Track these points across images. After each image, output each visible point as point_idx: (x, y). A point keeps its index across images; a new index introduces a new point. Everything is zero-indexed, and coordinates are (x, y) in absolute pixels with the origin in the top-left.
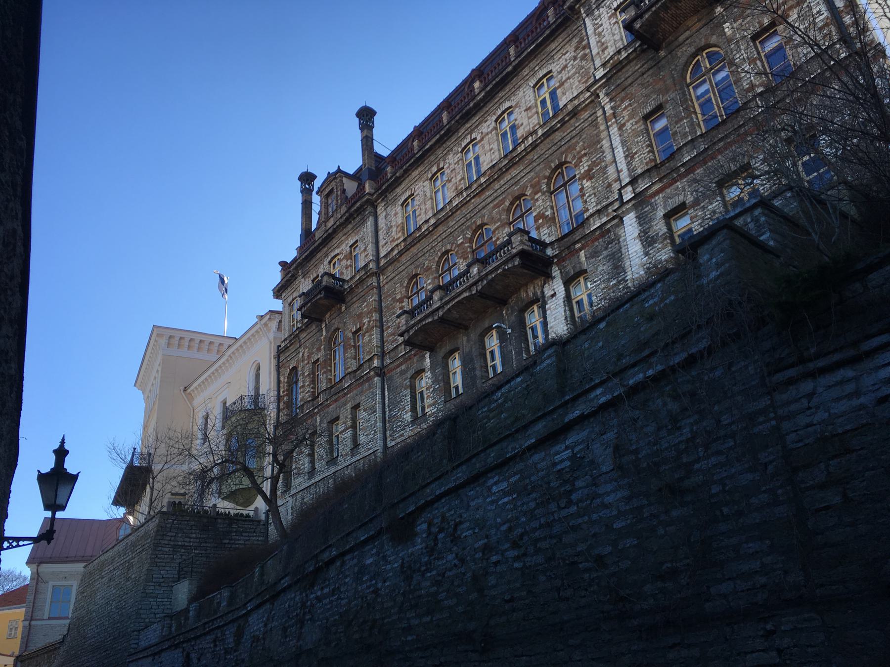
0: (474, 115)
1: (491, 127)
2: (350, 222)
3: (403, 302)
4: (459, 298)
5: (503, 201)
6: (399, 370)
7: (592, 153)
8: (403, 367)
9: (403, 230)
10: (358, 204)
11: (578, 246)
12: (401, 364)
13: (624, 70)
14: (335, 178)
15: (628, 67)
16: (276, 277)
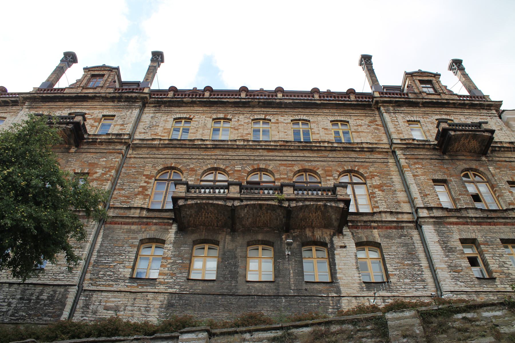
0: (273, 108)
1: (286, 121)
2: (113, 102)
3: (150, 179)
4: (215, 202)
5: (292, 166)
6: (126, 227)
7: (383, 178)
8: (134, 227)
9: (170, 133)
10: (134, 95)
11: (373, 224)
12: (133, 224)
13: (418, 150)
14: (111, 71)
15: (421, 150)
16: (85, 67)
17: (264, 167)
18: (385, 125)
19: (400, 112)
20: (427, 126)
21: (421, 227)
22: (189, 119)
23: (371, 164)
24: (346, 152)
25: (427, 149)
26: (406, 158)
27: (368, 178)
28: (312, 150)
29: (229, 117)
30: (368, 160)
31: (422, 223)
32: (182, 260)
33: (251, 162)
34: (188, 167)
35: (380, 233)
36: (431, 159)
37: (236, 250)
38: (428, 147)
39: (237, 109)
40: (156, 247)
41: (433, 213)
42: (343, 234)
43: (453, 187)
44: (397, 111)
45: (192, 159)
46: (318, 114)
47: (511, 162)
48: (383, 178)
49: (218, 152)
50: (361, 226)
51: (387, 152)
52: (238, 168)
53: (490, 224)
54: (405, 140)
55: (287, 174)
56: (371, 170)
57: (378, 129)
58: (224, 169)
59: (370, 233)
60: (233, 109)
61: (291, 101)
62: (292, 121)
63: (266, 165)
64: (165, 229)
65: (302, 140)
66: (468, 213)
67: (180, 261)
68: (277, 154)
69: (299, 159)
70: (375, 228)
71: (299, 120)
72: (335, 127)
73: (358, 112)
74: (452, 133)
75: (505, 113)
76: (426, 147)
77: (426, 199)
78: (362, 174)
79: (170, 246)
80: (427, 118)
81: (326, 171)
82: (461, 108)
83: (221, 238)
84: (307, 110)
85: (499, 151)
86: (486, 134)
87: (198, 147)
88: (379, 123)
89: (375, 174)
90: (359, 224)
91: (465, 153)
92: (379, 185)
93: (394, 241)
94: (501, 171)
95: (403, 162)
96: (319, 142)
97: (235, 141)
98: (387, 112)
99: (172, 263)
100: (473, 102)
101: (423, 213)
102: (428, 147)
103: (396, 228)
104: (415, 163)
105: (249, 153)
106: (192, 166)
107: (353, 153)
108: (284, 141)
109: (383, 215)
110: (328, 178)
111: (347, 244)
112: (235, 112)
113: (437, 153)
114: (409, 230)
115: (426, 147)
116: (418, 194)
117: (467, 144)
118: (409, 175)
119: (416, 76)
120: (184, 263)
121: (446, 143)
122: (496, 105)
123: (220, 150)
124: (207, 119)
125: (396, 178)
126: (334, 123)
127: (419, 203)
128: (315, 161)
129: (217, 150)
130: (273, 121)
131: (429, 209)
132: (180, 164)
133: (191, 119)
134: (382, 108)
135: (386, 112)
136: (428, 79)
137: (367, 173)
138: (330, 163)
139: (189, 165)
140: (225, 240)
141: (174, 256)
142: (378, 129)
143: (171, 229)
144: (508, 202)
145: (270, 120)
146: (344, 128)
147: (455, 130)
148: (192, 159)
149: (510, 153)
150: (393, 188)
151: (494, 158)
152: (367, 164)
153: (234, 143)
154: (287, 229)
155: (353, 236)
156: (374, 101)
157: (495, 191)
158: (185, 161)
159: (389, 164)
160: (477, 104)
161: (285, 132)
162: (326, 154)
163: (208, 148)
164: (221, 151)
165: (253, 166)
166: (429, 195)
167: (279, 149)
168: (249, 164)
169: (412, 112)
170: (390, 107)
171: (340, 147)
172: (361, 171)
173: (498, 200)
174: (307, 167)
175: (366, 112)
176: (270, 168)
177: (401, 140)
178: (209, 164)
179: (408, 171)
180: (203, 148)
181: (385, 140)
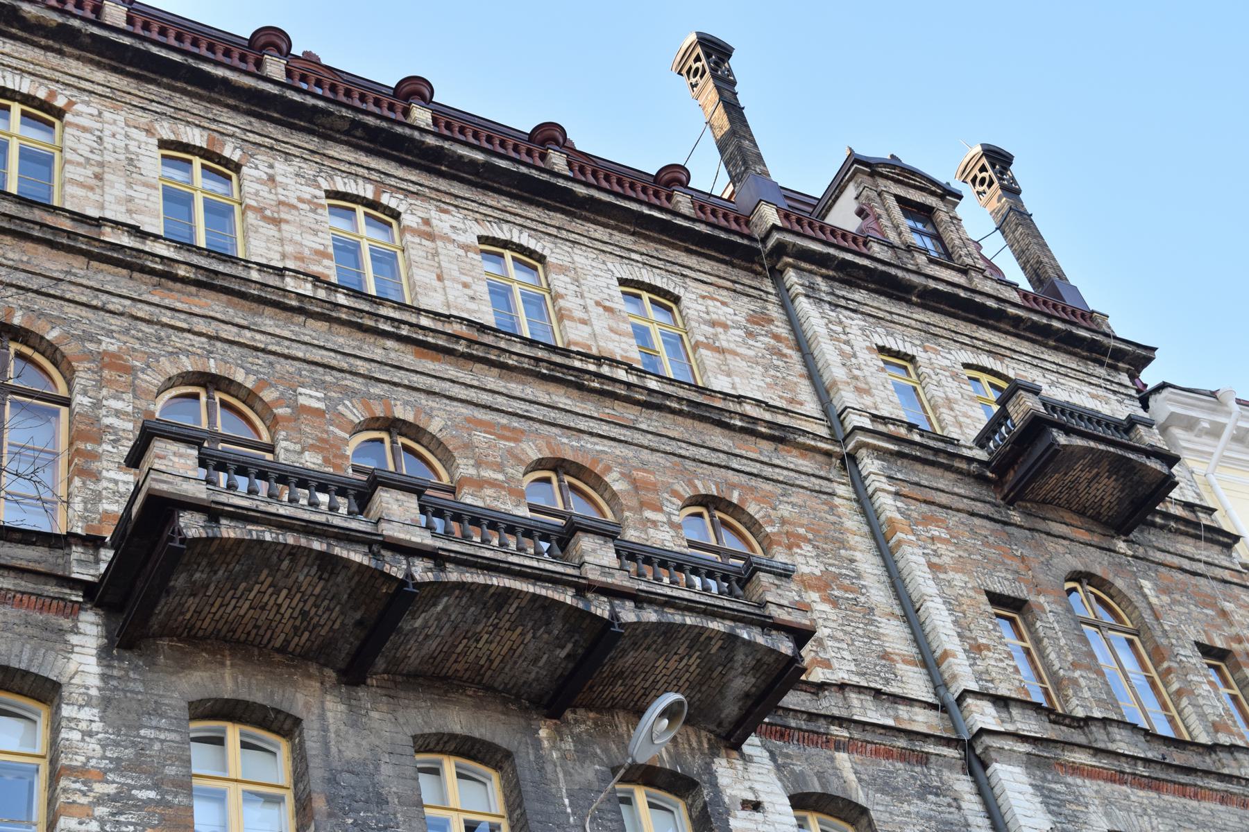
1: (462, 238)
5: (516, 436)
11: (835, 730)
13: (929, 469)
15: (939, 472)
17: (410, 417)
18: (803, 345)
19: (852, 305)
20: (939, 384)
21: (985, 766)
22: (45, 106)
23: (778, 489)
24: (696, 423)
25: (958, 471)
26: (897, 494)
27: (779, 544)
28: (580, 387)
29: (230, 151)
30: (768, 471)
31: (993, 755)
32: (156, 786)
33: (357, 384)
34: (91, 346)
35: (859, 768)
36: (972, 514)
37: (377, 767)
38: (964, 466)
39: (257, 125)
40: (245, 745)
41: (1012, 721)
42: (743, 756)
43: (1050, 633)
44: (843, 302)
45: (102, 309)
46: (572, 237)
47: (1194, 574)
48: (825, 552)
49: (214, 305)
50: (800, 730)
51: (828, 454)
52: (310, 398)
53: (1182, 790)
54: (884, 420)
55: (500, 467)
56: (786, 514)
57: (782, 355)
58: (250, 392)
59: (828, 764)
60: (240, 120)
61: (480, 157)
62: (482, 239)
63: (419, 410)
64: (45, 627)
65: (201, 242)
66: (1113, 741)
67: (152, 794)
68: (452, 372)
69: (535, 412)
70: (839, 746)
71: (506, 244)
72: (340, 224)
73: (707, 265)
74: (1062, 439)
75: (1166, 393)
76: (957, 464)
77: (981, 665)
78: (756, 522)
79: (86, 714)
80: (937, 352)
81: (636, 485)
82: (1033, 341)
83: (307, 705)
84: (533, 212)
85: (1162, 527)
86: (1154, 464)
87: (576, 383)
88: (783, 330)
89: (802, 531)
90: (793, 723)
91: (1068, 516)
92: (818, 578)
93: (906, 807)
94: (1174, 602)
95: (887, 505)
96: (599, 360)
97: (280, 272)
98: (811, 293)
99: (112, 798)
100: (1075, 330)
101: (983, 716)
102: (964, 466)
103: (904, 756)
104: (926, 520)
105: (343, 339)
106: (109, 345)
107: (718, 430)
108: (471, 323)
109: (854, 698)
110: (649, 514)
111: (763, 798)
112: (252, 137)
113: (985, 493)
114: (946, 774)
115: (957, 464)
116: (957, 640)
117: (1084, 484)
118: (913, 560)
119: (886, 177)
120: (168, 805)
121: (1026, 468)
122: (1139, 356)
123: (224, 297)
124: (134, 133)
125: (868, 564)
126: (175, 150)
127: (963, 675)
128: (591, 434)
129: (213, 295)
130: (407, 219)
131: (1002, 702)
132: (54, 322)
133: (60, 113)
134: (791, 277)
135: (807, 296)
136: (925, 202)
137: (772, 524)
138: (645, 455)
139: (92, 339)
140: (322, 717)
141: (119, 766)
142: (782, 355)
143: (75, 631)
144: (1211, 718)
145: (396, 215)
146: (217, 187)
147: (1068, 431)
148: (102, 309)
149: (1191, 541)
150: (863, 599)
151: (1151, 553)
152: (768, 487)
153: (273, 280)
154: (554, 701)
155: (779, 768)
156: (771, 243)
157: (1169, 670)
158: (72, 311)
159: (837, 501)
160: (1085, 339)
161: (466, 285)
162: (629, 413)
163: (175, 278)
164: (229, 304)
165: (367, 406)
166: (987, 648)
167: (463, 355)
168: (350, 393)
169: (888, 317)
170: (819, 280)
171: (680, 399)
172: (752, 509)
173: (1176, 706)
174: (569, 456)
175: (735, 273)
176: (434, 427)
177: (875, 418)
178: (188, 353)
179: (910, 543)
180: (152, 272)
181: (811, 406)
